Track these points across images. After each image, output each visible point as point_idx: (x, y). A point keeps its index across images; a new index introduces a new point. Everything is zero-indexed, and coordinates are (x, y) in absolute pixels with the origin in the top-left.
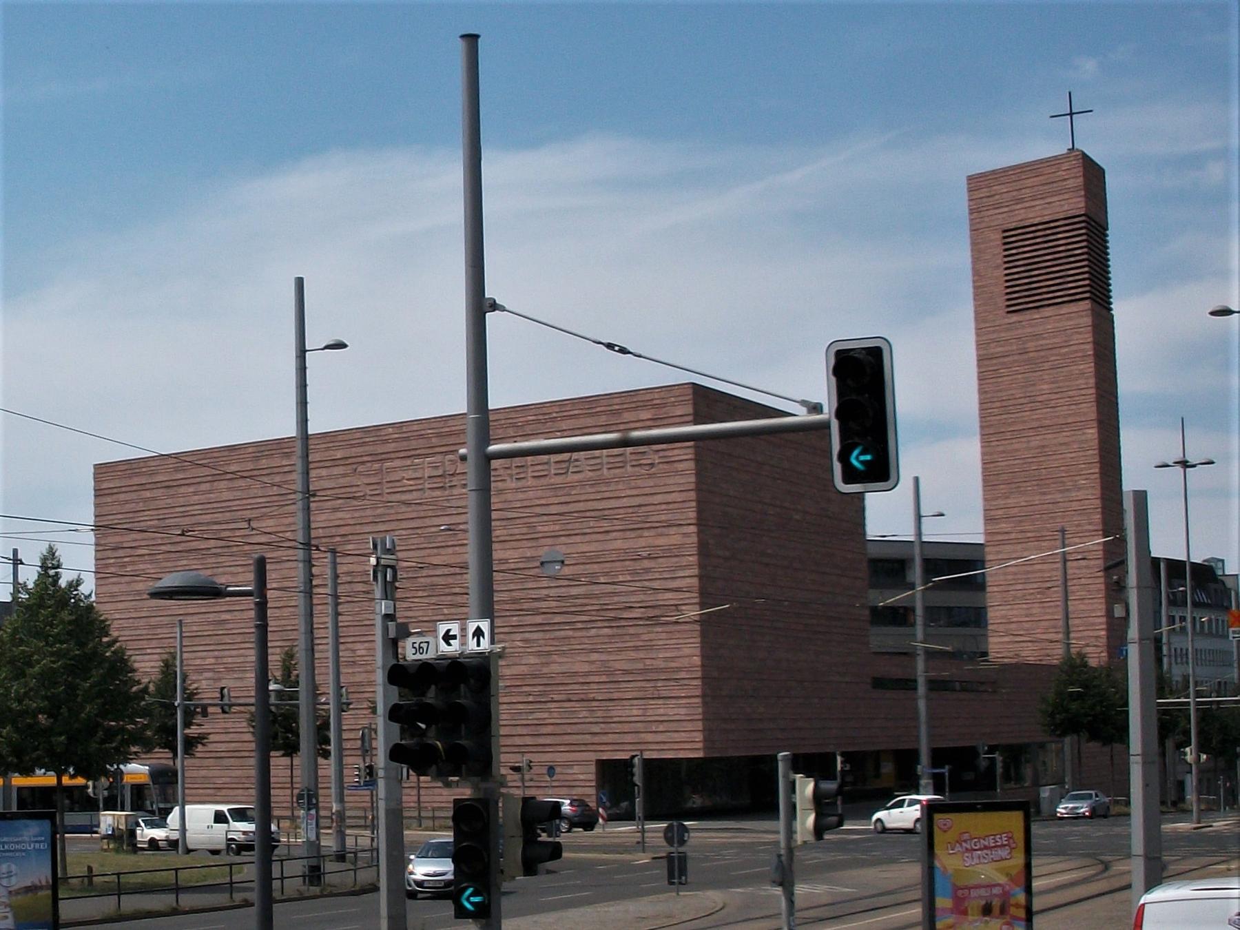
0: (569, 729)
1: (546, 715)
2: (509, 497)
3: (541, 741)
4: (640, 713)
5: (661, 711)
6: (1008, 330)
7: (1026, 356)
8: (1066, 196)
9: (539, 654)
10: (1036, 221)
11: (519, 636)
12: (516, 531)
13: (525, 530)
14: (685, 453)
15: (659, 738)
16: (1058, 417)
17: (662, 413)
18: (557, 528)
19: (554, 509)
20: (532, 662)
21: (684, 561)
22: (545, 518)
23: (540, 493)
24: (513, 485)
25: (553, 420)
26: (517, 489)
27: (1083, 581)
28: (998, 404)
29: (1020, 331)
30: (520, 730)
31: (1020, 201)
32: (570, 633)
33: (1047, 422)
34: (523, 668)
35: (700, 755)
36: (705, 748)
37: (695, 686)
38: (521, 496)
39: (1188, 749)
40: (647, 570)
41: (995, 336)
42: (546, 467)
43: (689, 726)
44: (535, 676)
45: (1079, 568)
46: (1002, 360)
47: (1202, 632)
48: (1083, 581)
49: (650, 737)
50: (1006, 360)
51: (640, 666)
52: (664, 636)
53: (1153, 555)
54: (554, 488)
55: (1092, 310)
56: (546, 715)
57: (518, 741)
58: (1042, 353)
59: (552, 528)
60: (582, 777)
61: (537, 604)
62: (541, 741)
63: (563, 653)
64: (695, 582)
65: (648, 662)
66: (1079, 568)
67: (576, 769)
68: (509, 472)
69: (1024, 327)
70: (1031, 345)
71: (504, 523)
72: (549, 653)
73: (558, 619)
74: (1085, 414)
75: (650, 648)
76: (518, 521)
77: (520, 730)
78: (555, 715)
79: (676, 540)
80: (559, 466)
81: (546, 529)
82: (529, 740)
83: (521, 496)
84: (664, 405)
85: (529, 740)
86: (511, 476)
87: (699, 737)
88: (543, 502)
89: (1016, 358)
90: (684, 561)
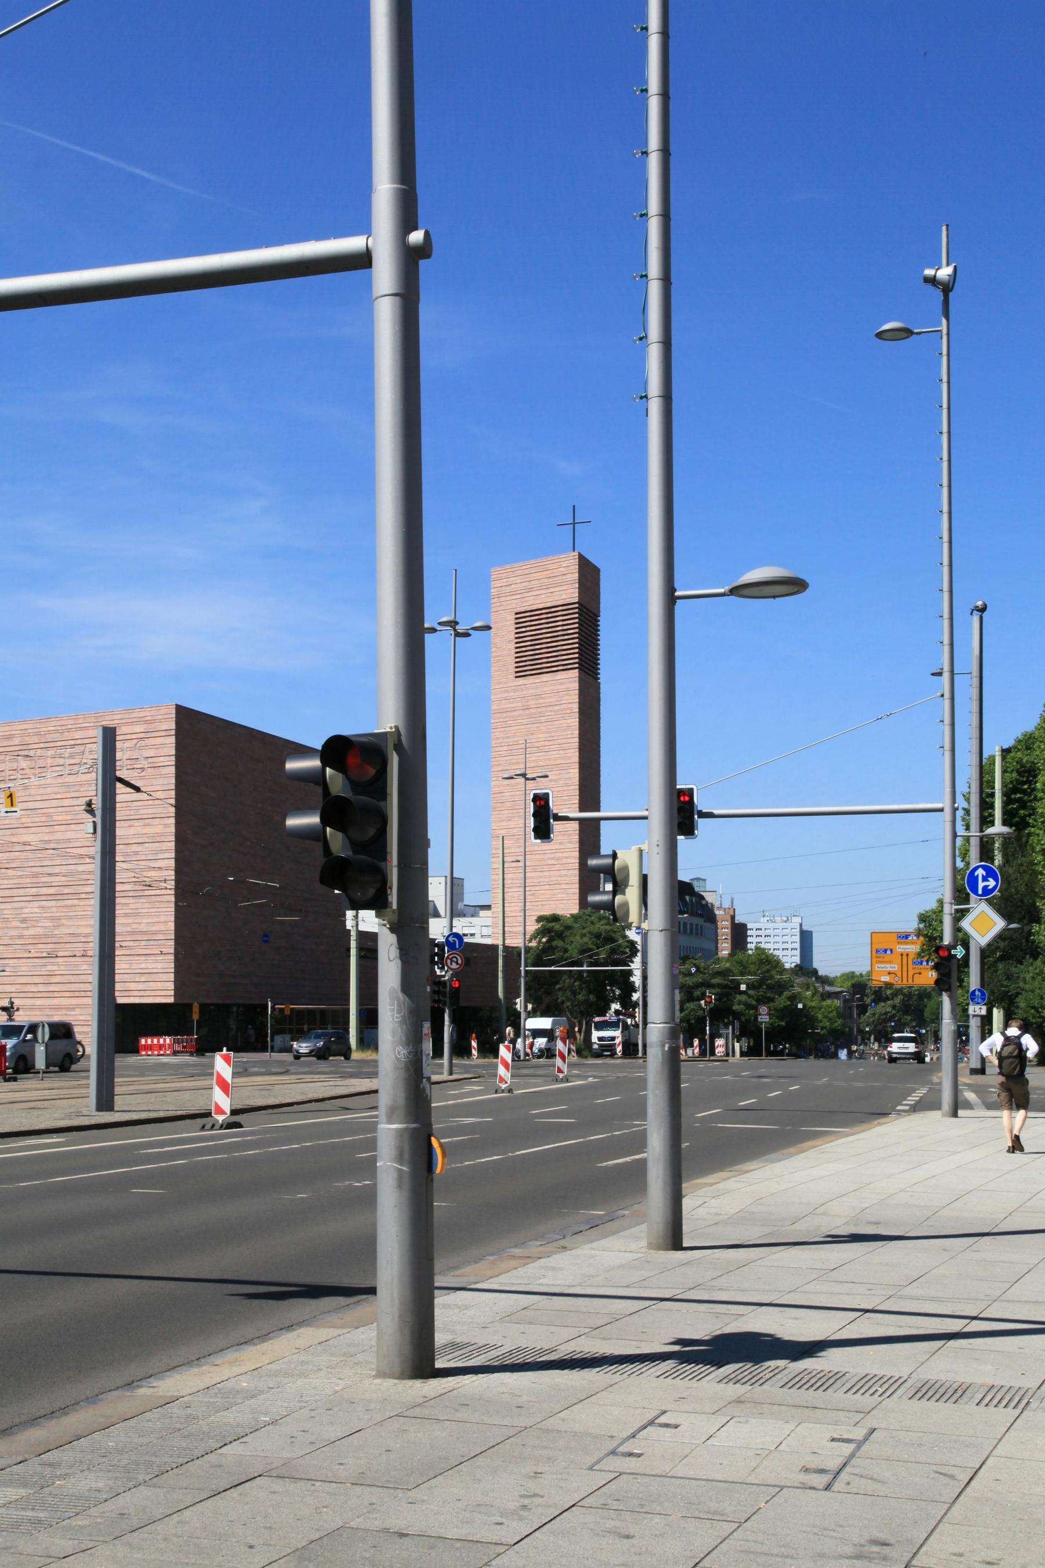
0: (73, 979)
1: (55, 968)
2: (33, 792)
3: (51, 988)
4: (127, 966)
5: (143, 966)
6: (515, 691)
7: (527, 712)
8: (564, 588)
9: (52, 919)
10: (541, 606)
11: (36, 904)
12: (38, 819)
13: (44, 819)
14: (575, 825)
15: (141, 986)
16: (549, 759)
17: (151, 727)
18: (69, 817)
19: (66, 802)
20: (46, 925)
21: (164, 846)
22: (60, 809)
23: (56, 790)
24: (36, 783)
25: (69, 730)
26: (39, 786)
27: (563, 886)
28: (505, 748)
29: (525, 692)
30: (36, 980)
31: (530, 590)
32: (76, 902)
33: (542, 764)
34: (39, 929)
35: (171, 1000)
36: (175, 996)
37: (170, 947)
38: (42, 791)
39: (518, 1000)
40: (136, 853)
41: (506, 695)
42: (61, 768)
43: (164, 977)
44: (47, 936)
45: (560, 876)
46: (509, 714)
47: (685, 932)
48: (563, 886)
49: (133, 986)
50: (513, 714)
51: (129, 929)
52: (147, 905)
53: (680, 878)
54: (68, 786)
55: (580, 677)
56: (55, 968)
57: (33, 988)
58: (539, 710)
59: (65, 817)
60: (82, 1018)
61: (52, 879)
62: (51, 988)
63: (71, 918)
64: (172, 863)
65: (134, 926)
66: (560, 876)
67: (77, 1012)
68: (33, 771)
69: (527, 689)
70: (532, 703)
71: (29, 812)
72: (59, 919)
73: (67, 890)
74: (570, 758)
75: (137, 915)
76: (39, 811)
77: (36, 980)
78: (62, 968)
79: (159, 829)
80: (71, 767)
81: (60, 818)
82: (41, 988)
83: (42, 791)
84: (154, 721)
85: (41, 988)
86: (35, 775)
87: (171, 986)
88: (59, 796)
89: (521, 712)
90: (164, 846)
